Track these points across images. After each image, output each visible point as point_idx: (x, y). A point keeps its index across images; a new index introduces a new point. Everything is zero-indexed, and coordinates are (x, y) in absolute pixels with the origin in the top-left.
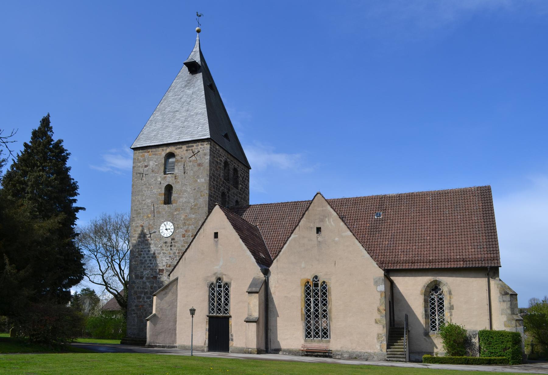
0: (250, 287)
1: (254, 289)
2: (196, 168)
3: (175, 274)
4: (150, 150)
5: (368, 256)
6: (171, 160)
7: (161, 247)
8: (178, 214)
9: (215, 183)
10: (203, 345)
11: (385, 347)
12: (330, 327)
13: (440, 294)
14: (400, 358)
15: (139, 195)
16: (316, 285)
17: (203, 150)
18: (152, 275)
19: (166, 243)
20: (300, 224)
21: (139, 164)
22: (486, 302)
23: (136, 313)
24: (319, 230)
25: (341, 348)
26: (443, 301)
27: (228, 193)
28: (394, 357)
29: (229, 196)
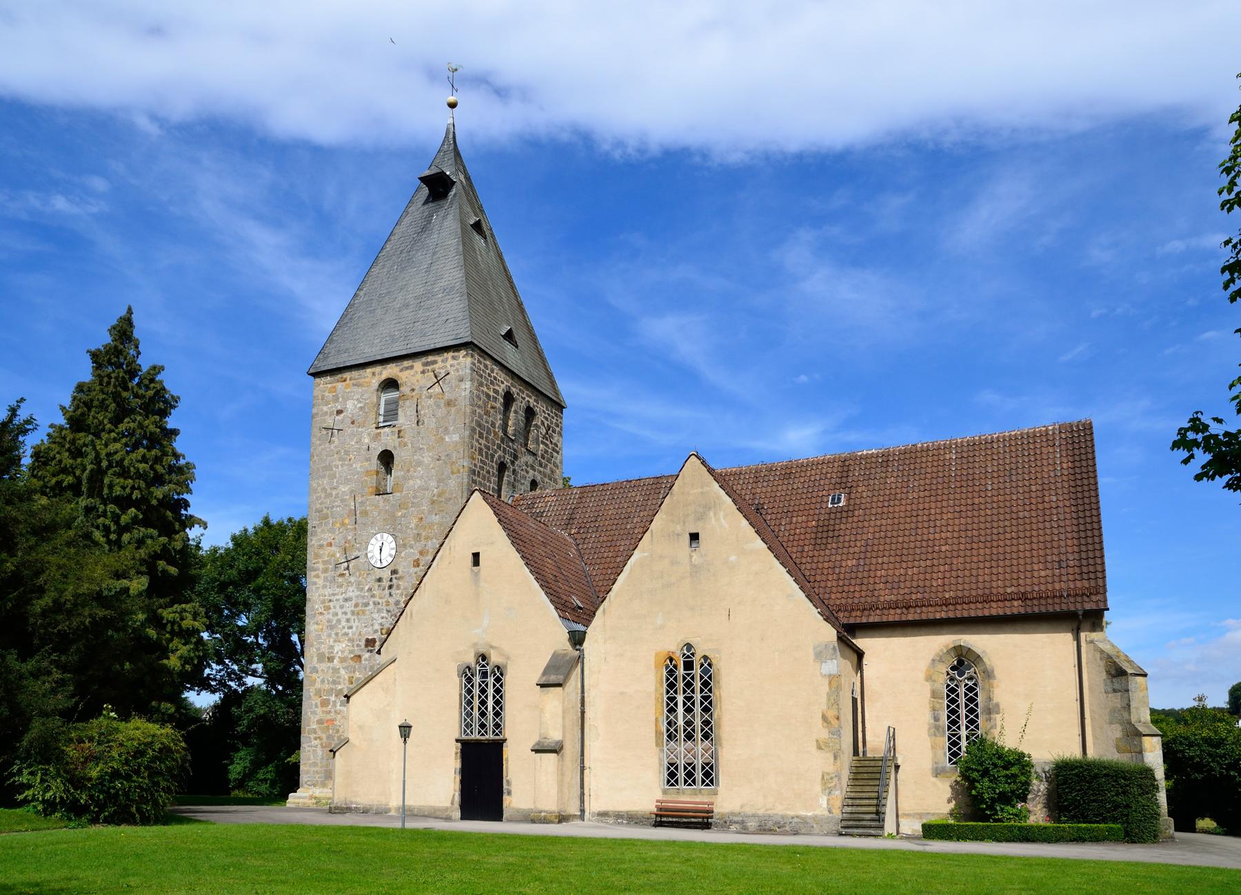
0: (544, 673)
1: (553, 678)
2: (442, 412)
3: (390, 648)
5: (802, 595)
7: (370, 589)
8: (404, 516)
9: (483, 442)
10: (448, 804)
12: (717, 760)
14: (870, 827)
15: (324, 477)
16: (689, 665)
17: (457, 370)
18: (351, 652)
19: (380, 580)
21: (325, 409)
23: (320, 738)
24: (694, 537)
27: (513, 463)
28: (857, 827)
29: (514, 471)
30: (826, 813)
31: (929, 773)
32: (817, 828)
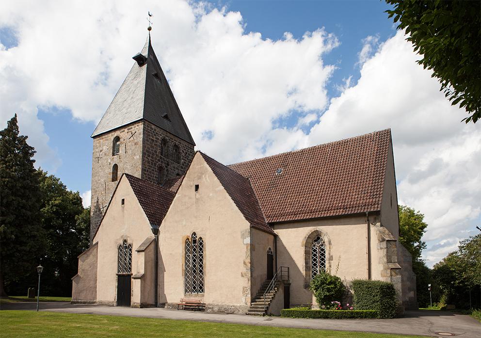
2: (133, 147)
4: (104, 137)
6: (118, 143)
11: (250, 300)
13: (322, 245)
20: (182, 184)
22: (366, 250)
24: (197, 187)
25: (213, 301)
26: (325, 252)
28: (254, 311)
29: (167, 170)
30: (244, 304)
31: (303, 287)
32: (241, 312)
